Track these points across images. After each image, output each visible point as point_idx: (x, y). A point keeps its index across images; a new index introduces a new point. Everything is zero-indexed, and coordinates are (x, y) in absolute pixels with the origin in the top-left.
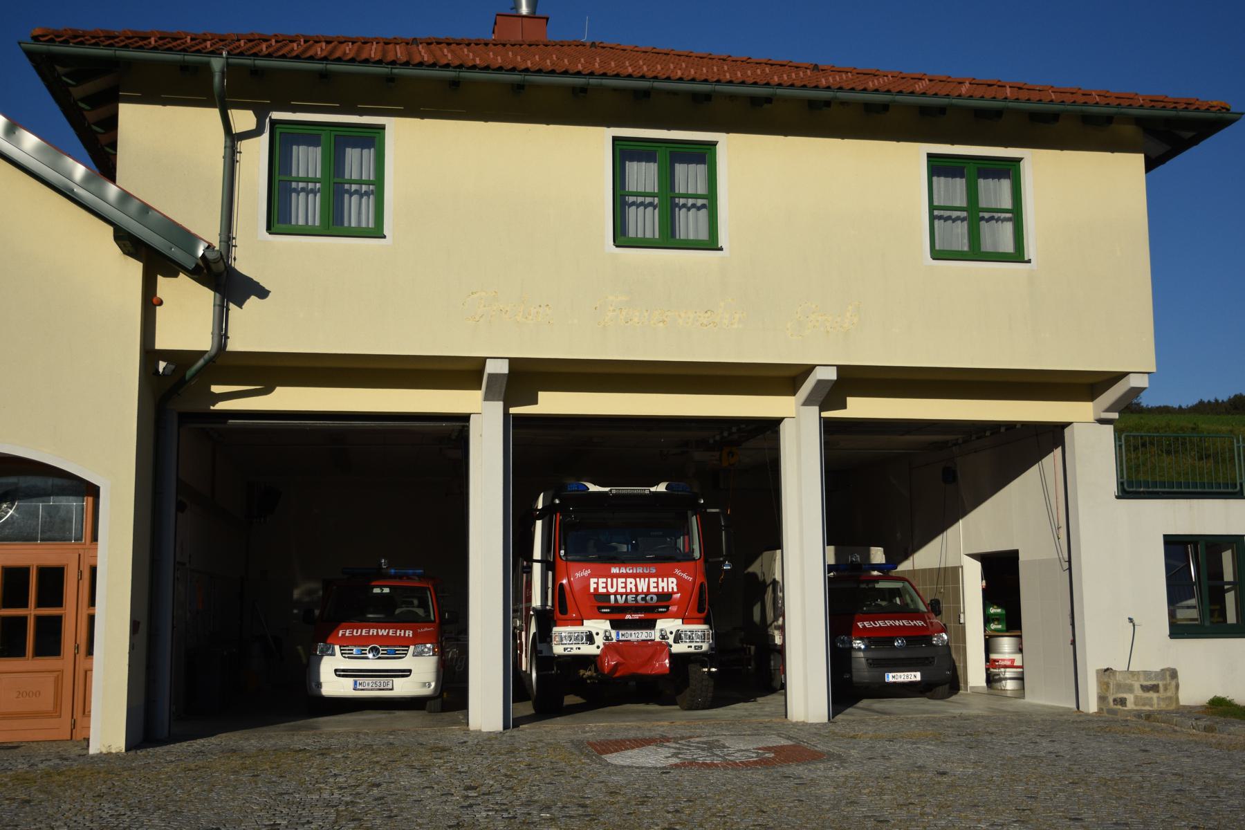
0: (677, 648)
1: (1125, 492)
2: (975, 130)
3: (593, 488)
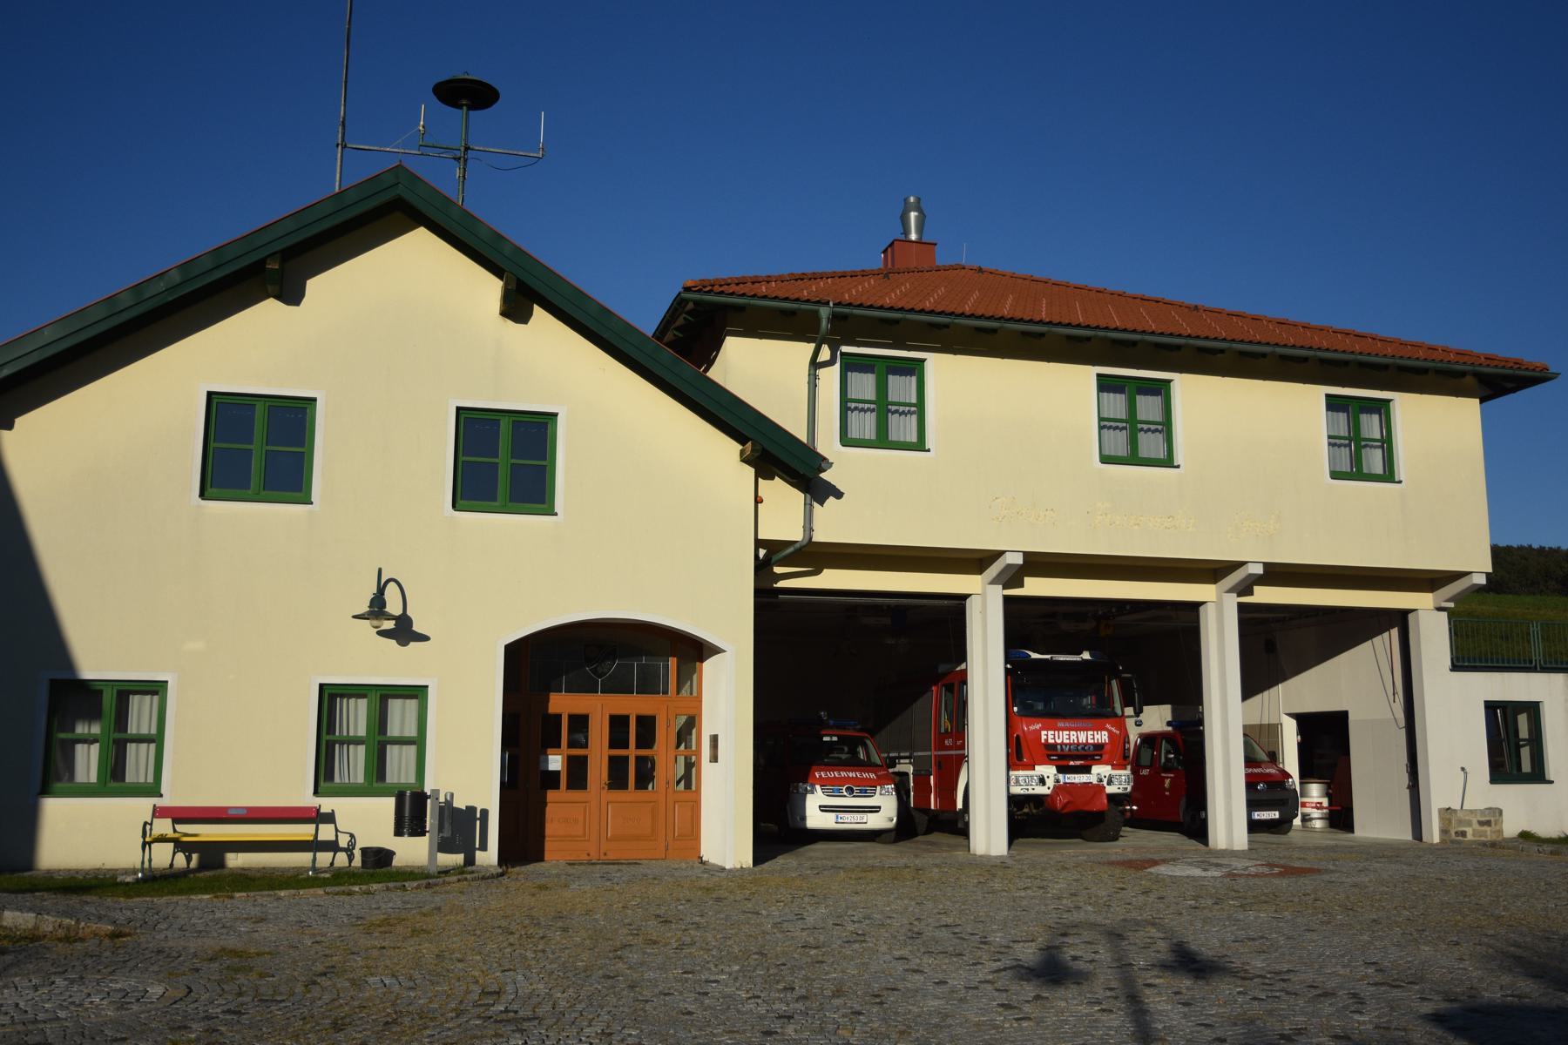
0: (1110, 790)
1: (1455, 667)
2: (1361, 373)
3: (1035, 656)
